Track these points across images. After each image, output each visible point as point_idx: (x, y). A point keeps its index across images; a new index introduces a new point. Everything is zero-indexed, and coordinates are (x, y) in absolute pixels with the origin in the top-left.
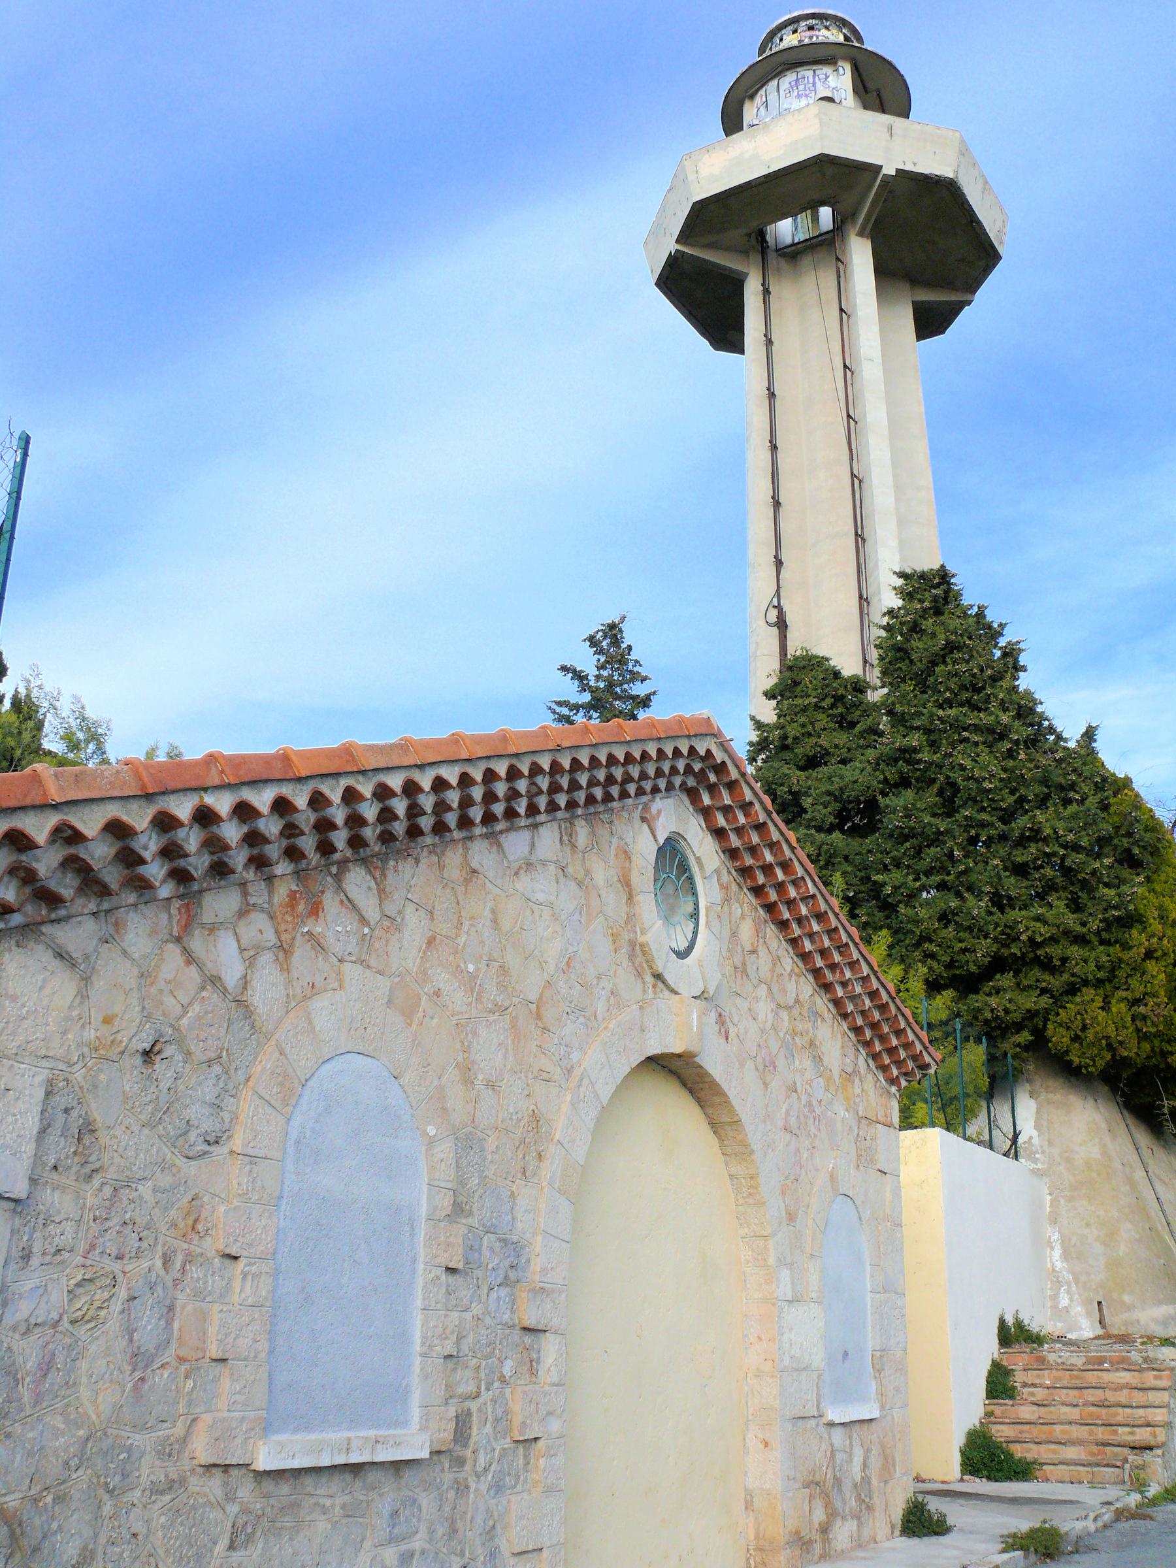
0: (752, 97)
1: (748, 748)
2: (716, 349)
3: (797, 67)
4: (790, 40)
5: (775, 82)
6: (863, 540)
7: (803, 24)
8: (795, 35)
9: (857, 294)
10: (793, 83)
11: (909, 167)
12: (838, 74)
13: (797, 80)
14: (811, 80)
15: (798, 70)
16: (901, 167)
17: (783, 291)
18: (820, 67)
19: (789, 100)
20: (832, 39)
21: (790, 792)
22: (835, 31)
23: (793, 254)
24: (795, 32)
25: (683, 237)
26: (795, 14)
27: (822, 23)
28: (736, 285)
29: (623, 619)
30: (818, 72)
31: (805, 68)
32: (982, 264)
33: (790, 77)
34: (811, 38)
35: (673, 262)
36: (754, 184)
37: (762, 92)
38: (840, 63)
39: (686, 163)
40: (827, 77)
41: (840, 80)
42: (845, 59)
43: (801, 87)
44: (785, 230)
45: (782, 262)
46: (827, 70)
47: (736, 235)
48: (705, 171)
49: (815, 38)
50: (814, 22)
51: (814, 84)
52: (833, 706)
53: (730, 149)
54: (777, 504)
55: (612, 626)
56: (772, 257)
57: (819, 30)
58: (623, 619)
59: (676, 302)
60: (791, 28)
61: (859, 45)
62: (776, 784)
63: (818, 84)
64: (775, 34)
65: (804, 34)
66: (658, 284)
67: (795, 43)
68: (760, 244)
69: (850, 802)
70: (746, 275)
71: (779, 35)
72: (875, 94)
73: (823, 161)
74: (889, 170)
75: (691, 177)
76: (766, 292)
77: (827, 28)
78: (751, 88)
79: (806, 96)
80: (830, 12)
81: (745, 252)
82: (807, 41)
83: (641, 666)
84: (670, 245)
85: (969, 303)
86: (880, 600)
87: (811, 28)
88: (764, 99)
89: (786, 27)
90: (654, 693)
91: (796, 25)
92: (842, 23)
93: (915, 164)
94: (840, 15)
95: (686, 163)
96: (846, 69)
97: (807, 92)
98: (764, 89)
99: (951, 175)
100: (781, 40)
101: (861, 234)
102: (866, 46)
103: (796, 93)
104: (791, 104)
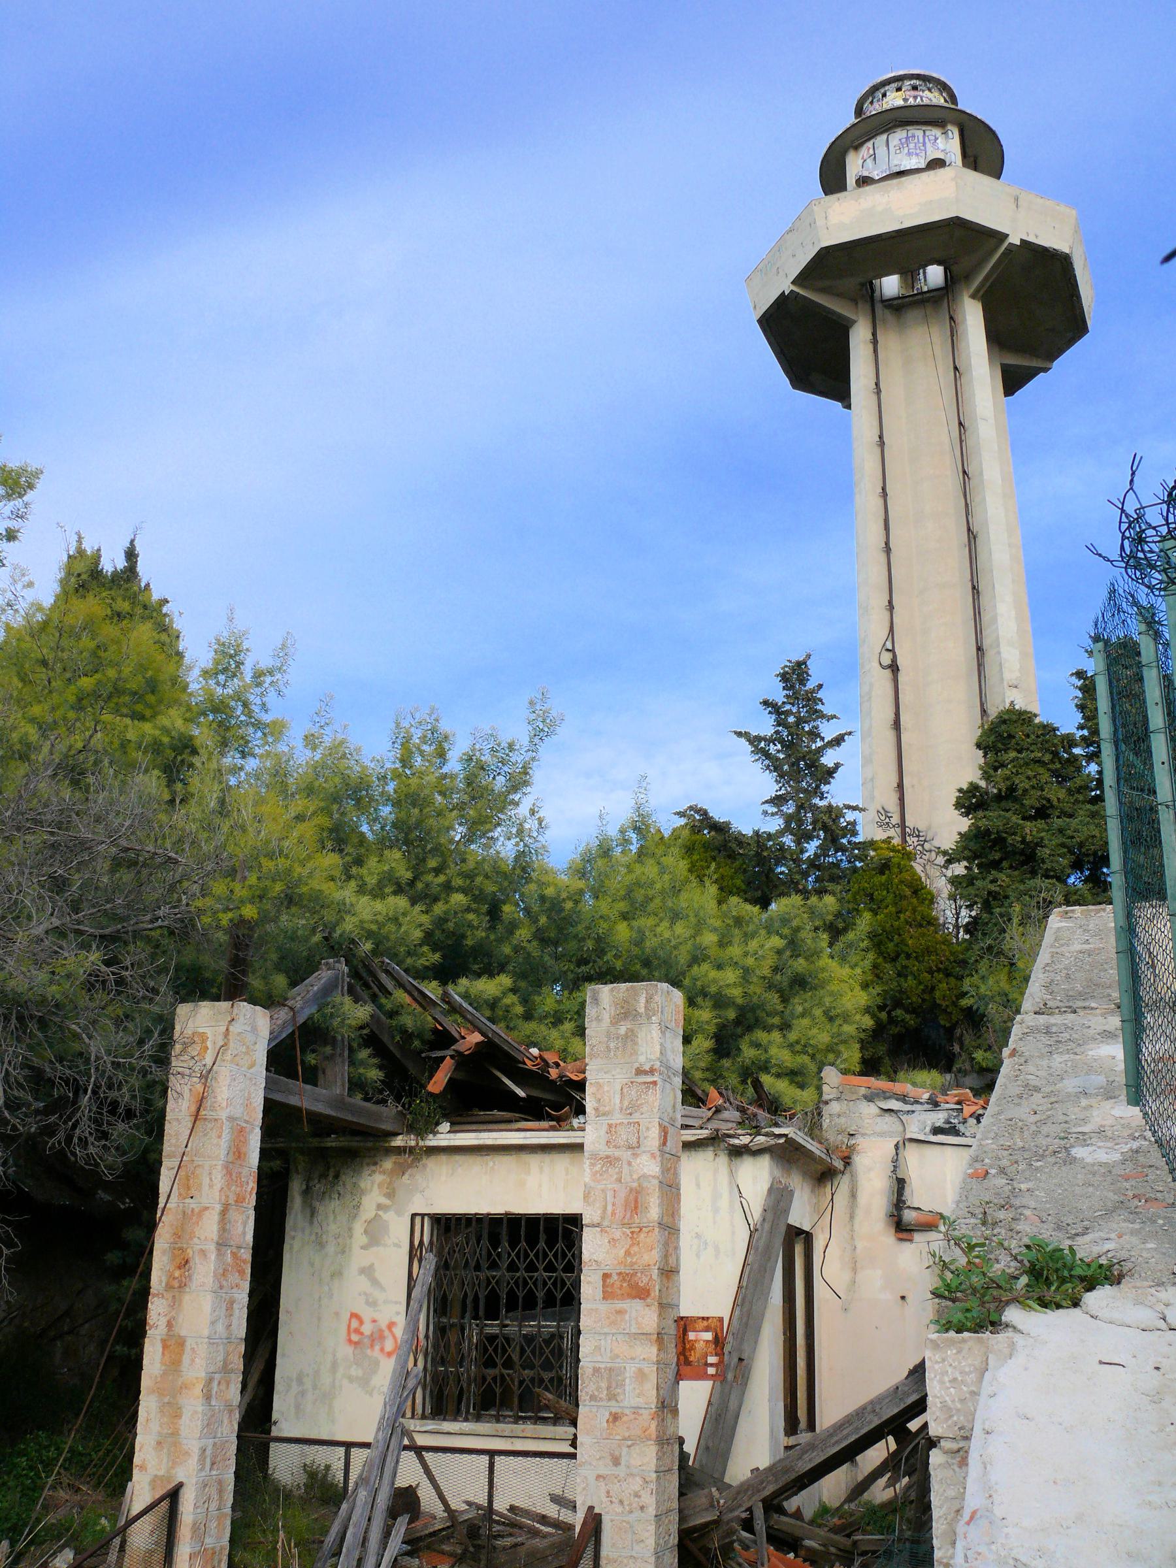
0: (857, 148)
1: (957, 794)
2: (794, 387)
3: (908, 125)
4: (894, 99)
5: (884, 137)
6: (978, 592)
7: (907, 83)
8: (900, 93)
9: (972, 354)
10: (904, 140)
11: (1031, 239)
12: (947, 137)
13: (907, 138)
14: (921, 140)
15: (908, 128)
16: (1025, 238)
17: (890, 341)
18: (929, 128)
19: (899, 156)
20: (935, 102)
21: (1023, 841)
22: (937, 94)
23: (898, 306)
24: (899, 89)
25: (800, 280)
26: (901, 73)
27: (926, 85)
28: (840, 332)
29: (809, 656)
30: (928, 133)
31: (915, 127)
32: (1070, 335)
33: (898, 135)
34: (915, 98)
35: (782, 301)
36: (884, 237)
37: (870, 144)
38: (949, 127)
39: (815, 208)
40: (936, 139)
41: (948, 144)
42: (954, 123)
43: (912, 146)
44: (891, 285)
45: (887, 312)
46: (936, 132)
47: (850, 284)
48: (834, 219)
49: (919, 99)
50: (918, 82)
51: (924, 144)
52: (1052, 762)
53: (862, 200)
54: (888, 549)
55: (799, 664)
56: (879, 307)
57: (923, 91)
58: (809, 656)
59: (772, 339)
60: (894, 85)
61: (953, 106)
62: (1006, 833)
63: (928, 144)
64: (878, 89)
65: (908, 93)
66: (760, 321)
67: (901, 103)
68: (868, 296)
69: (1088, 855)
70: (854, 322)
71: (882, 91)
72: (972, 159)
73: (957, 223)
74: (1015, 240)
75: (820, 222)
76: (875, 342)
77: (930, 90)
78: (857, 139)
79: (917, 154)
80: (935, 75)
81: (854, 301)
82: (911, 101)
83: (823, 704)
84: (785, 285)
85: (1046, 370)
86: (999, 653)
87: (915, 88)
88: (871, 152)
89: (889, 83)
90: (850, 733)
91: (900, 84)
92: (944, 87)
93: (1037, 237)
94: (942, 79)
95: (815, 208)
96: (954, 133)
97: (918, 151)
98: (871, 142)
99: (1067, 251)
100: (884, 95)
101: (973, 296)
102: (960, 107)
103: (906, 150)
104: (901, 160)
